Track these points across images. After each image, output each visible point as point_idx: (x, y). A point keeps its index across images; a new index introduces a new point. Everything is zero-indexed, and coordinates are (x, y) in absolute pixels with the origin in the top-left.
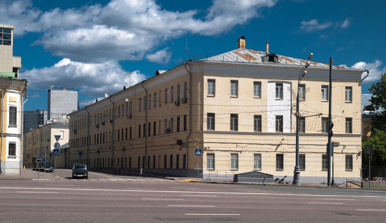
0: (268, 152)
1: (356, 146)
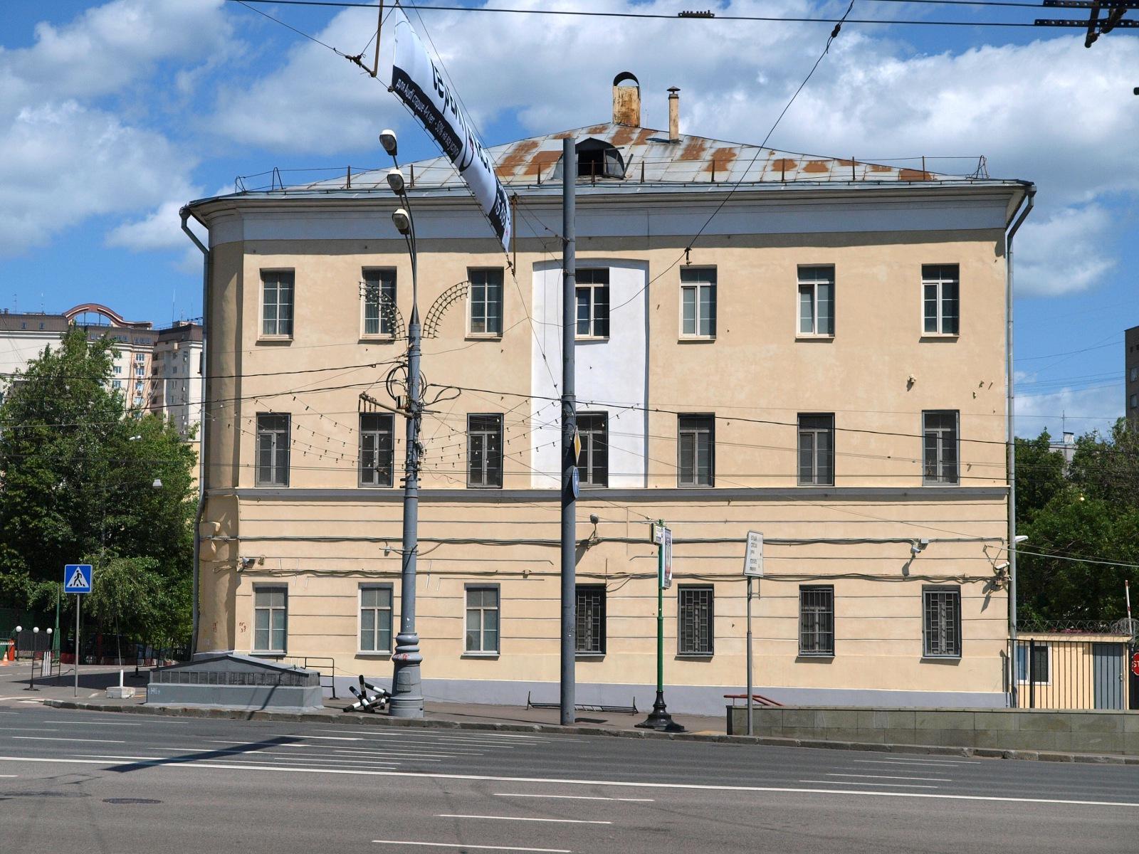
0: (529, 577)
1: (981, 545)
